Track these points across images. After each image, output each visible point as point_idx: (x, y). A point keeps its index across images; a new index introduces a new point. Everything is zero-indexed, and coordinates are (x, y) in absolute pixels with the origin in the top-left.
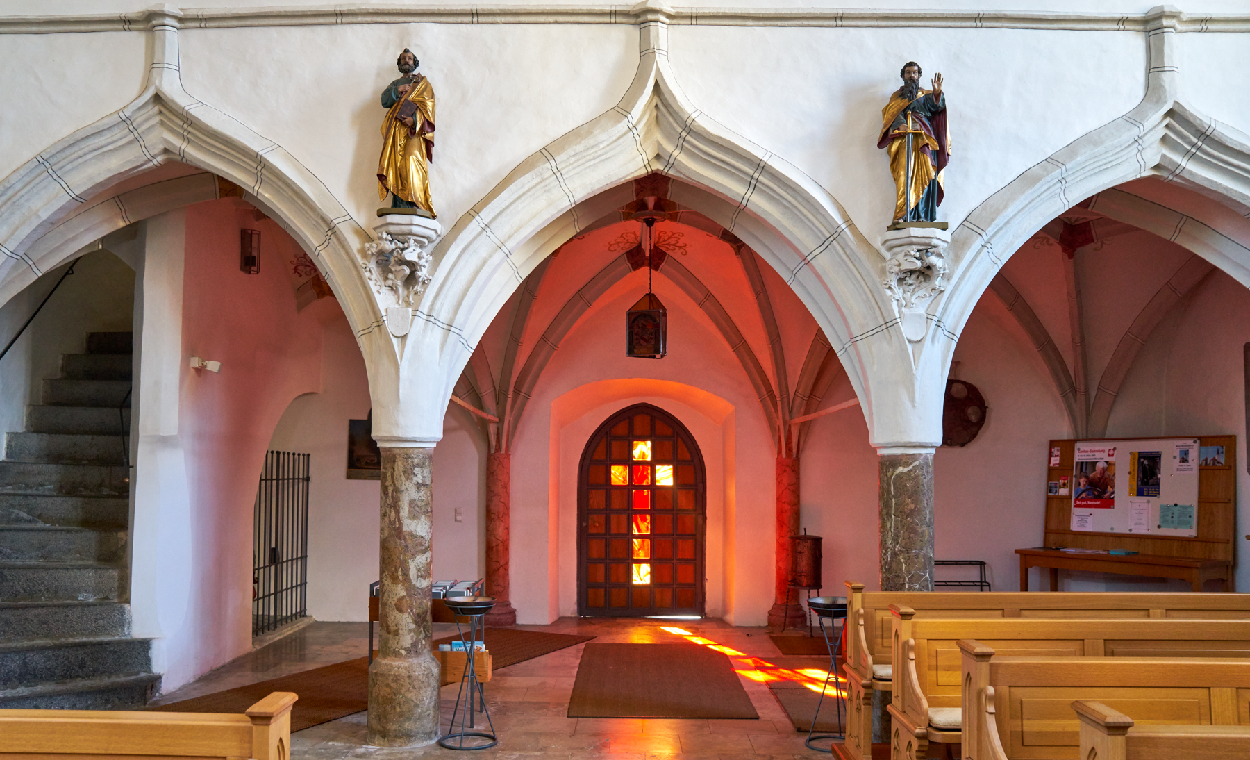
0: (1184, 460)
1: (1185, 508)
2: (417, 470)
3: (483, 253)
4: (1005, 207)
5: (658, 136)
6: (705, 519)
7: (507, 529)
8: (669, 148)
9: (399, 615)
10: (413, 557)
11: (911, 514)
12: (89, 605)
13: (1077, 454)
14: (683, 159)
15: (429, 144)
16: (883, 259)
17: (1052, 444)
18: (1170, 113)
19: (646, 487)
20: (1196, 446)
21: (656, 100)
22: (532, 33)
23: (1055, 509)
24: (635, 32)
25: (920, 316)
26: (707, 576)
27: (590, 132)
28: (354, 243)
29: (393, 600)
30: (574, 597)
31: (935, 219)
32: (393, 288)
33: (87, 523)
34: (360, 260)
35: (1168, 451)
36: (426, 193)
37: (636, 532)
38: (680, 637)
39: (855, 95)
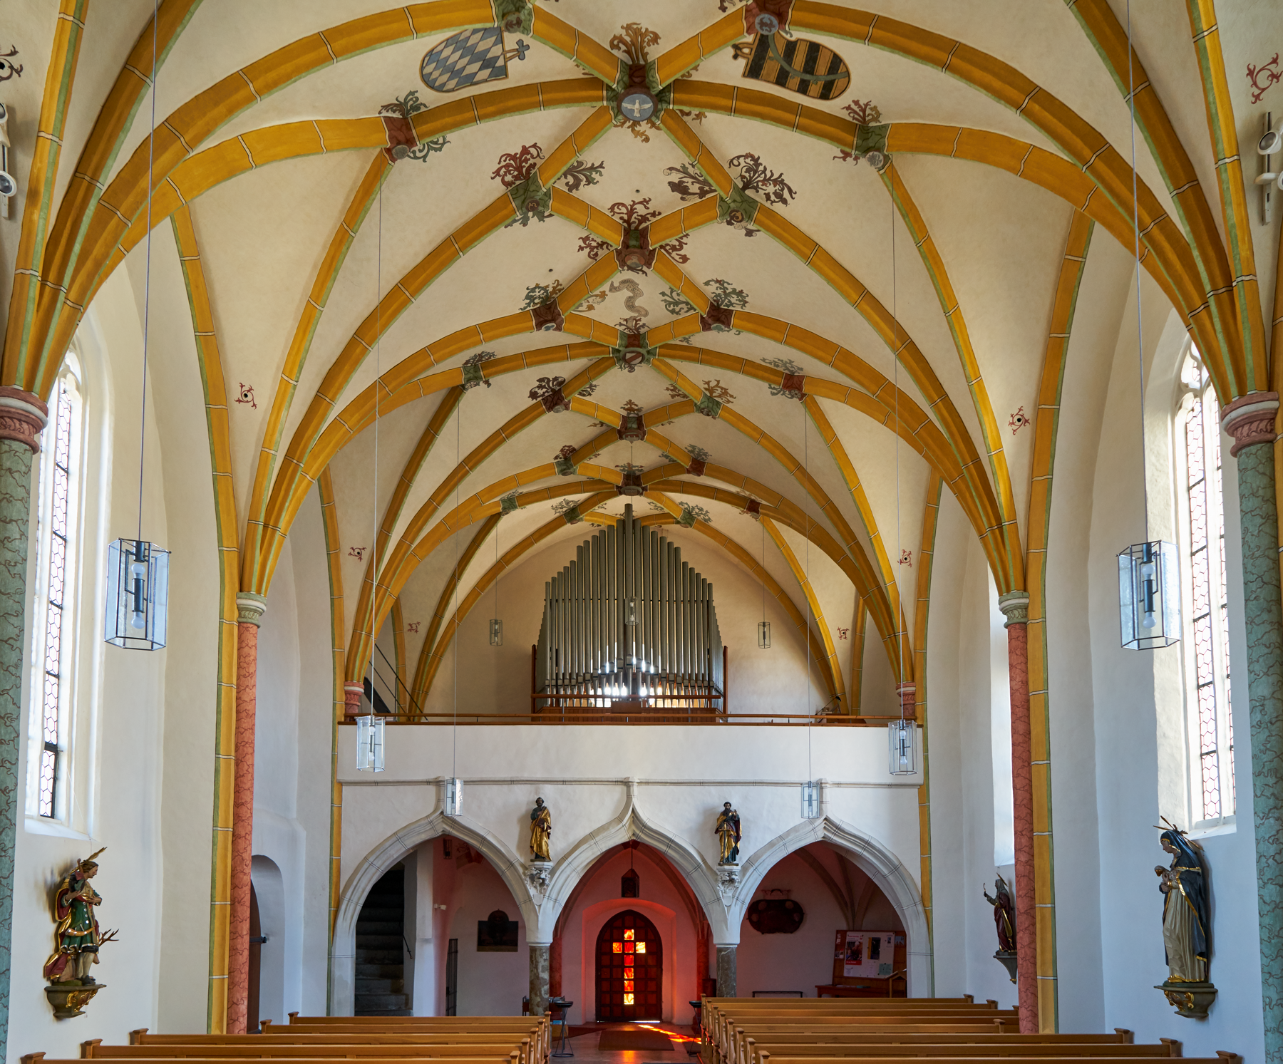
0: (889, 942)
1: (888, 965)
2: (544, 954)
3: (568, 873)
4: (762, 856)
5: (634, 828)
6: (662, 970)
7: (561, 976)
8: (638, 832)
9: (537, 1008)
10: (543, 986)
11: (726, 969)
12: (394, 1010)
13: (847, 937)
14: (643, 836)
15: (549, 834)
16: (717, 874)
17: (838, 932)
18: (825, 819)
19: (631, 954)
20: (894, 935)
21: (633, 815)
22: (586, 787)
23: (838, 965)
24: (625, 788)
25: (730, 896)
26: (663, 1000)
27: (608, 828)
28: (521, 870)
29: (535, 1003)
30: (594, 1012)
31: (735, 860)
32: (535, 887)
33: (383, 976)
34: (523, 877)
35: (883, 937)
36: (548, 852)
37: (626, 977)
38: (648, 1029)
39: (707, 812)
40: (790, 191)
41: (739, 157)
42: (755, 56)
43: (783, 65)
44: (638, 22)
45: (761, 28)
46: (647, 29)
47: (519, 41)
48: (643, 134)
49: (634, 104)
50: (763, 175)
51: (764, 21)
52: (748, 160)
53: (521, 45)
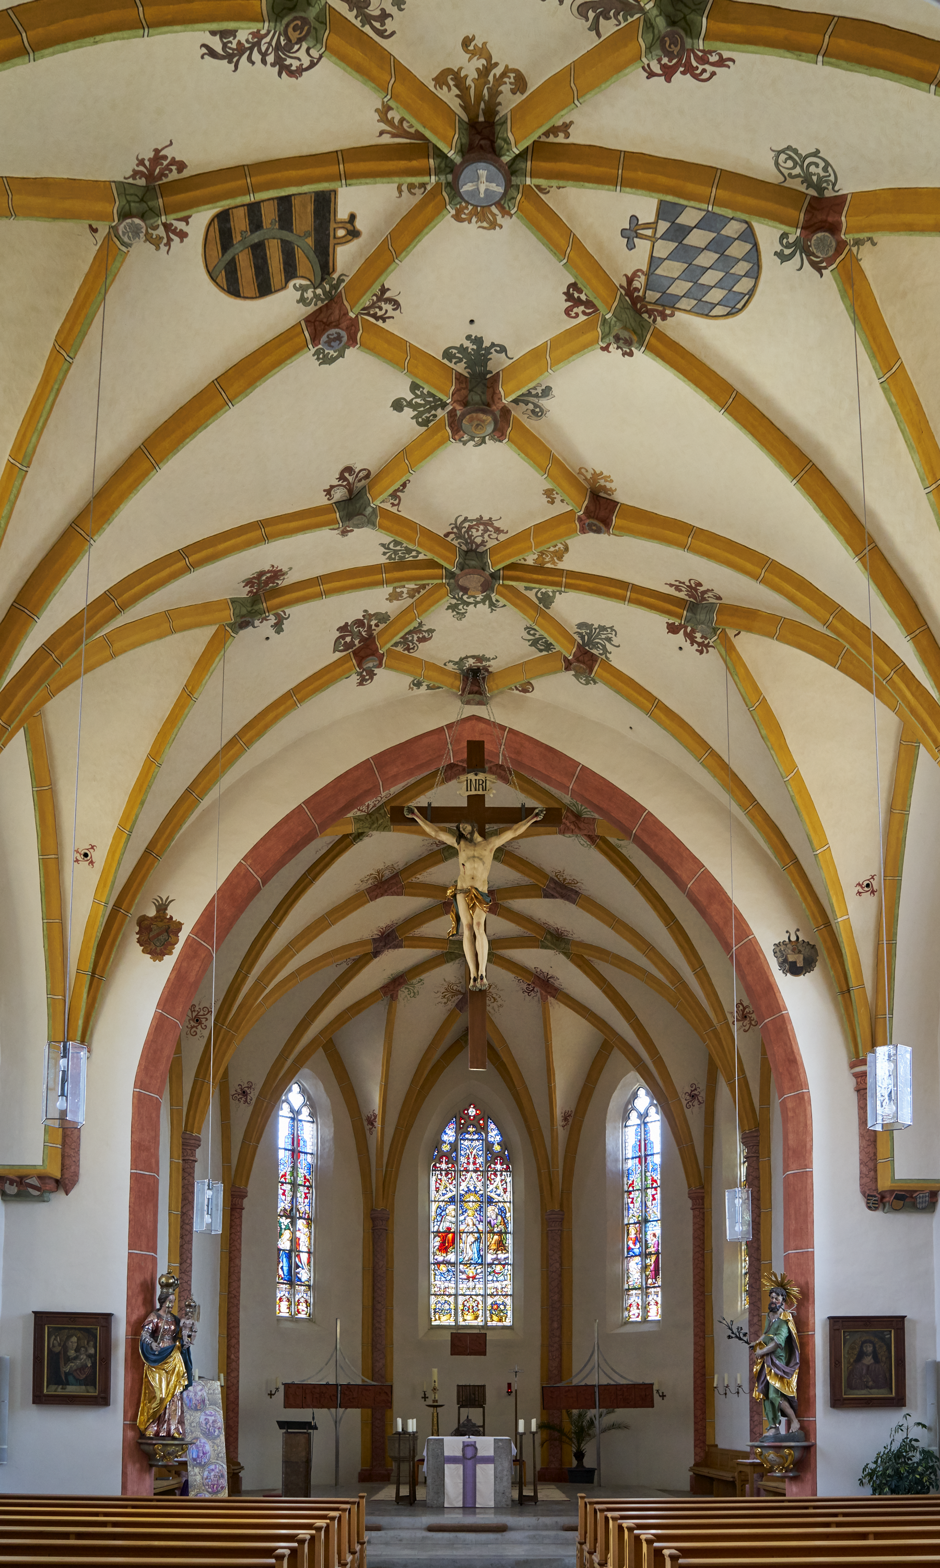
30: (360, 1351)
40: (212, 53)
41: (312, 65)
42: (328, 228)
43: (290, 234)
44: (481, 229)
45: (339, 334)
46: (470, 222)
47: (632, 249)
48: (473, 54)
49: (486, 190)
50: (263, 49)
51: (338, 342)
52: (295, 64)
53: (631, 240)
